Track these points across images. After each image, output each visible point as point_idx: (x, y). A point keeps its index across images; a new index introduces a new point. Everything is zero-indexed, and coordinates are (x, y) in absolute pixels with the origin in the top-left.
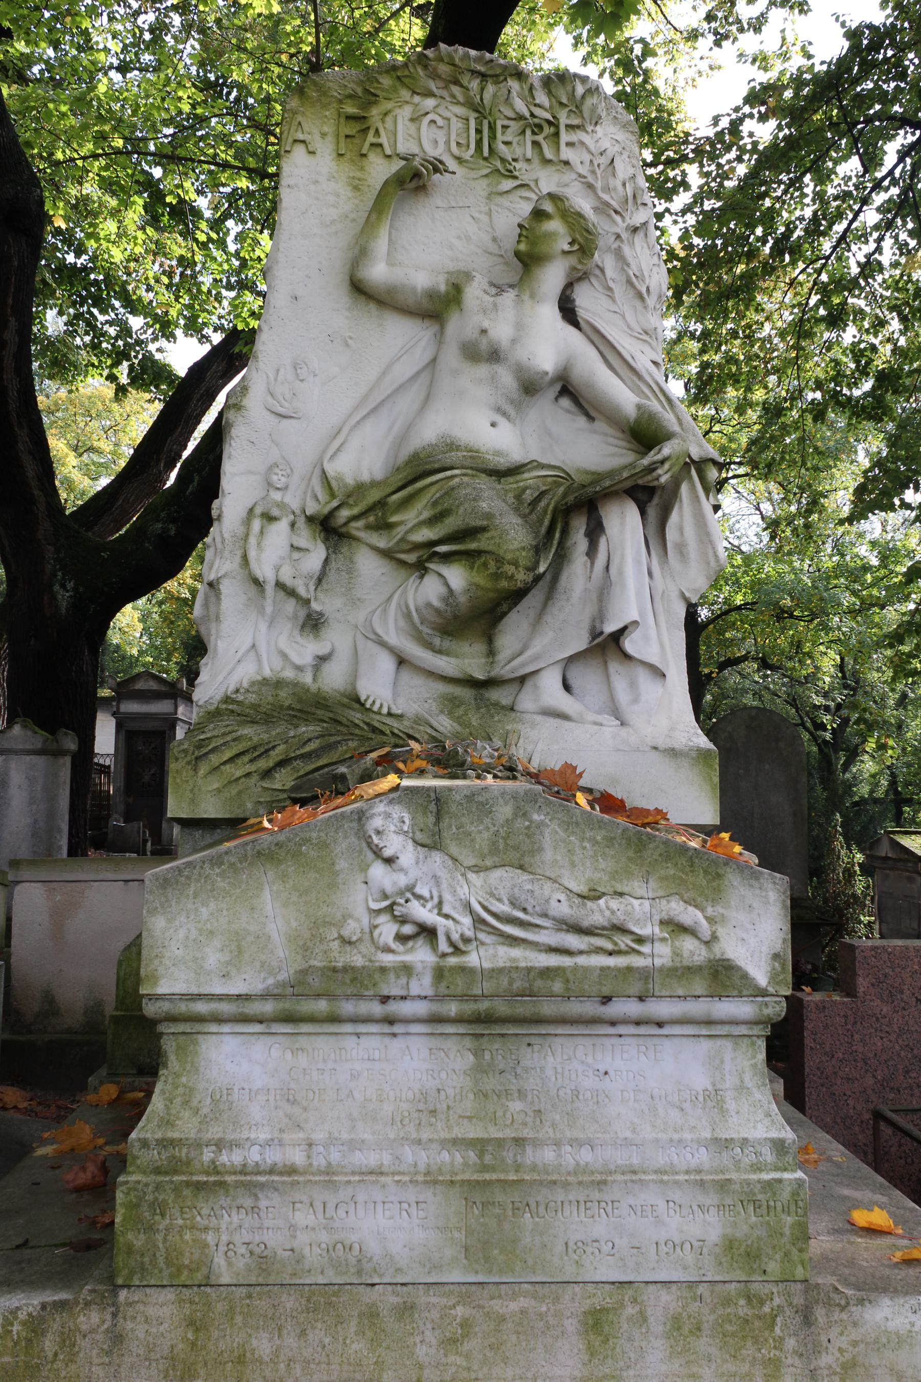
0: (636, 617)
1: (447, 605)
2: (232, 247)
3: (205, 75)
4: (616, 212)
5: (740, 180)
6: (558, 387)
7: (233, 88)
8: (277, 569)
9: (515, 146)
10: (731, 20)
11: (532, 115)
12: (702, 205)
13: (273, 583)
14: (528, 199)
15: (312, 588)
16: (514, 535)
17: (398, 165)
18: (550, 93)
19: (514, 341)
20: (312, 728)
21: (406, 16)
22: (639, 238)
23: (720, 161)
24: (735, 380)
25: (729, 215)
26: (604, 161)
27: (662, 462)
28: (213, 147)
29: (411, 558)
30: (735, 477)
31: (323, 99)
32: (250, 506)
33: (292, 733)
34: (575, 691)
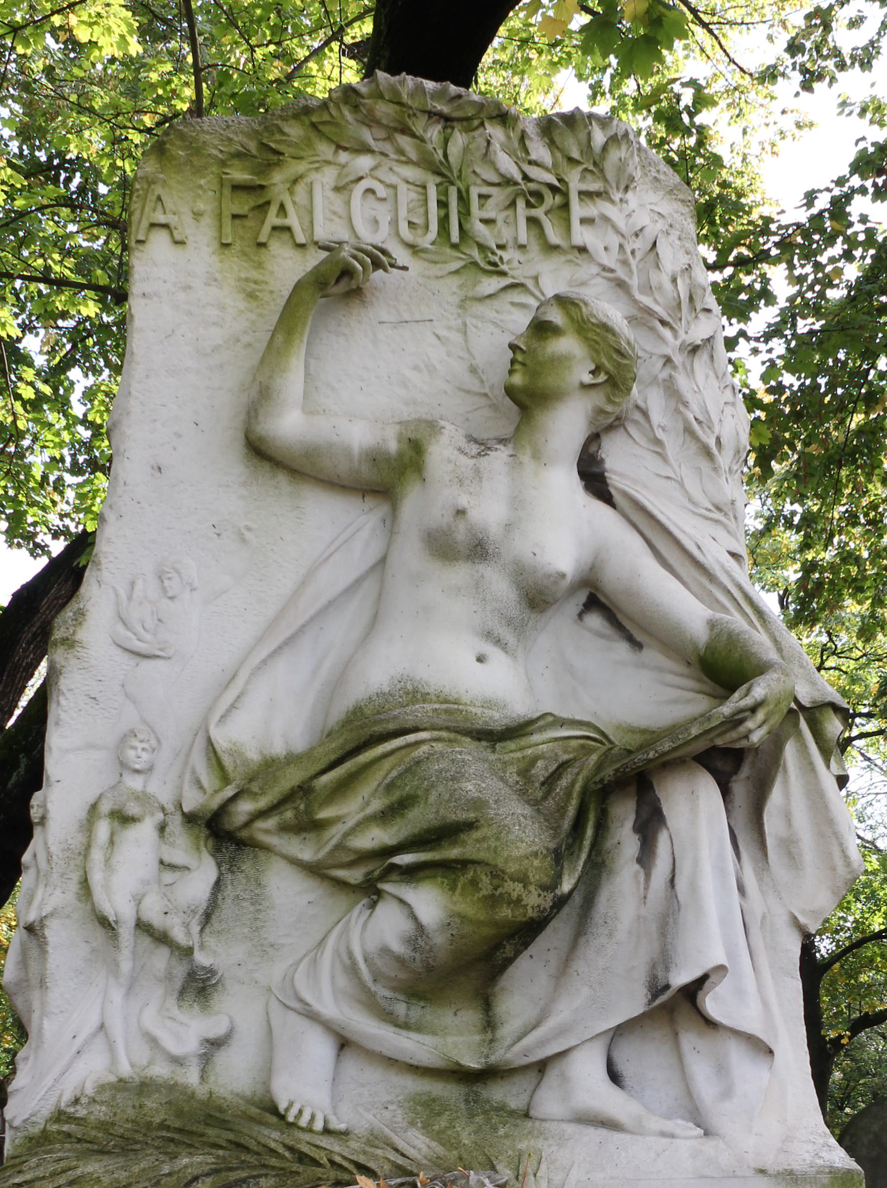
0: (722, 960)
1: (415, 949)
2: (78, 410)
3: (32, 154)
4: (663, 323)
5: (850, 288)
6: (582, 597)
7: (74, 171)
8: (138, 900)
9: (500, 225)
10: (825, 52)
11: (526, 177)
12: (794, 325)
13: (132, 923)
14: (523, 306)
15: (195, 928)
16: (520, 835)
17: (315, 258)
18: (552, 144)
19: (509, 527)
20: (199, 1159)
21: (335, 56)
22: (700, 363)
23: (819, 258)
24: (857, 588)
25: (836, 338)
26: (641, 245)
27: (753, 710)
28: (42, 256)
29: (355, 876)
30: (862, 736)
31: (195, 159)
32: (91, 800)
33: (166, 1169)
34: (628, 1082)
